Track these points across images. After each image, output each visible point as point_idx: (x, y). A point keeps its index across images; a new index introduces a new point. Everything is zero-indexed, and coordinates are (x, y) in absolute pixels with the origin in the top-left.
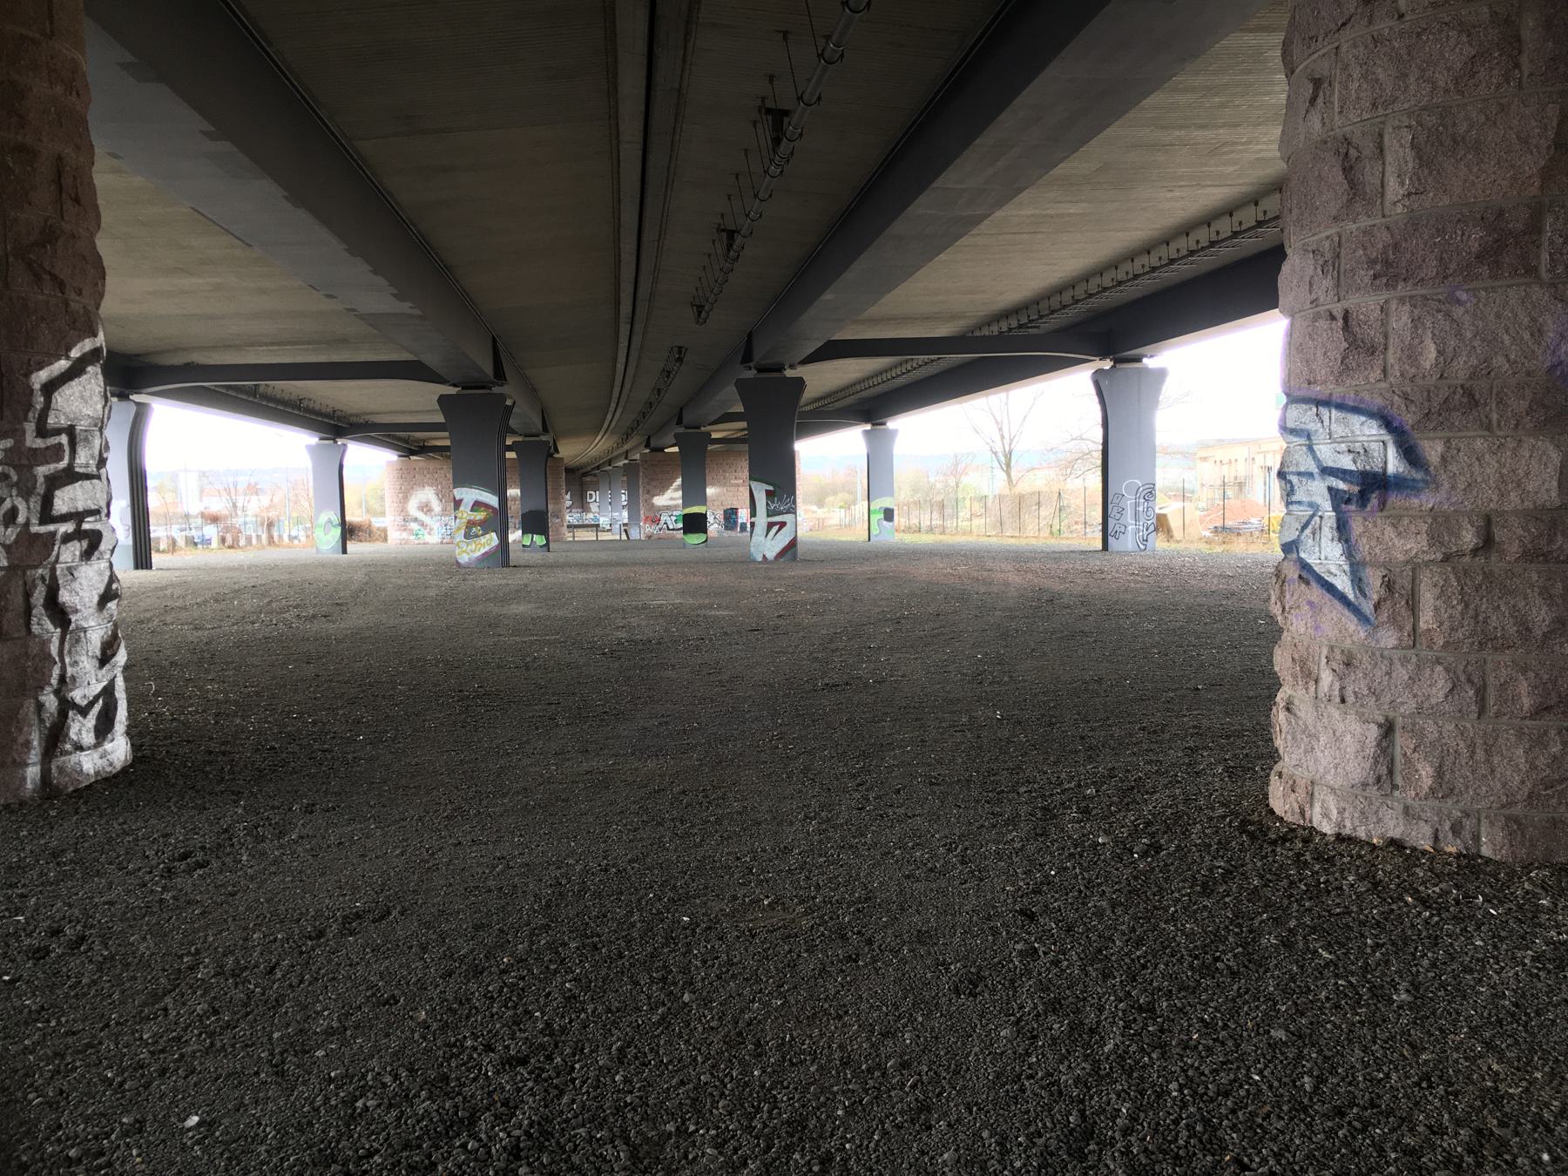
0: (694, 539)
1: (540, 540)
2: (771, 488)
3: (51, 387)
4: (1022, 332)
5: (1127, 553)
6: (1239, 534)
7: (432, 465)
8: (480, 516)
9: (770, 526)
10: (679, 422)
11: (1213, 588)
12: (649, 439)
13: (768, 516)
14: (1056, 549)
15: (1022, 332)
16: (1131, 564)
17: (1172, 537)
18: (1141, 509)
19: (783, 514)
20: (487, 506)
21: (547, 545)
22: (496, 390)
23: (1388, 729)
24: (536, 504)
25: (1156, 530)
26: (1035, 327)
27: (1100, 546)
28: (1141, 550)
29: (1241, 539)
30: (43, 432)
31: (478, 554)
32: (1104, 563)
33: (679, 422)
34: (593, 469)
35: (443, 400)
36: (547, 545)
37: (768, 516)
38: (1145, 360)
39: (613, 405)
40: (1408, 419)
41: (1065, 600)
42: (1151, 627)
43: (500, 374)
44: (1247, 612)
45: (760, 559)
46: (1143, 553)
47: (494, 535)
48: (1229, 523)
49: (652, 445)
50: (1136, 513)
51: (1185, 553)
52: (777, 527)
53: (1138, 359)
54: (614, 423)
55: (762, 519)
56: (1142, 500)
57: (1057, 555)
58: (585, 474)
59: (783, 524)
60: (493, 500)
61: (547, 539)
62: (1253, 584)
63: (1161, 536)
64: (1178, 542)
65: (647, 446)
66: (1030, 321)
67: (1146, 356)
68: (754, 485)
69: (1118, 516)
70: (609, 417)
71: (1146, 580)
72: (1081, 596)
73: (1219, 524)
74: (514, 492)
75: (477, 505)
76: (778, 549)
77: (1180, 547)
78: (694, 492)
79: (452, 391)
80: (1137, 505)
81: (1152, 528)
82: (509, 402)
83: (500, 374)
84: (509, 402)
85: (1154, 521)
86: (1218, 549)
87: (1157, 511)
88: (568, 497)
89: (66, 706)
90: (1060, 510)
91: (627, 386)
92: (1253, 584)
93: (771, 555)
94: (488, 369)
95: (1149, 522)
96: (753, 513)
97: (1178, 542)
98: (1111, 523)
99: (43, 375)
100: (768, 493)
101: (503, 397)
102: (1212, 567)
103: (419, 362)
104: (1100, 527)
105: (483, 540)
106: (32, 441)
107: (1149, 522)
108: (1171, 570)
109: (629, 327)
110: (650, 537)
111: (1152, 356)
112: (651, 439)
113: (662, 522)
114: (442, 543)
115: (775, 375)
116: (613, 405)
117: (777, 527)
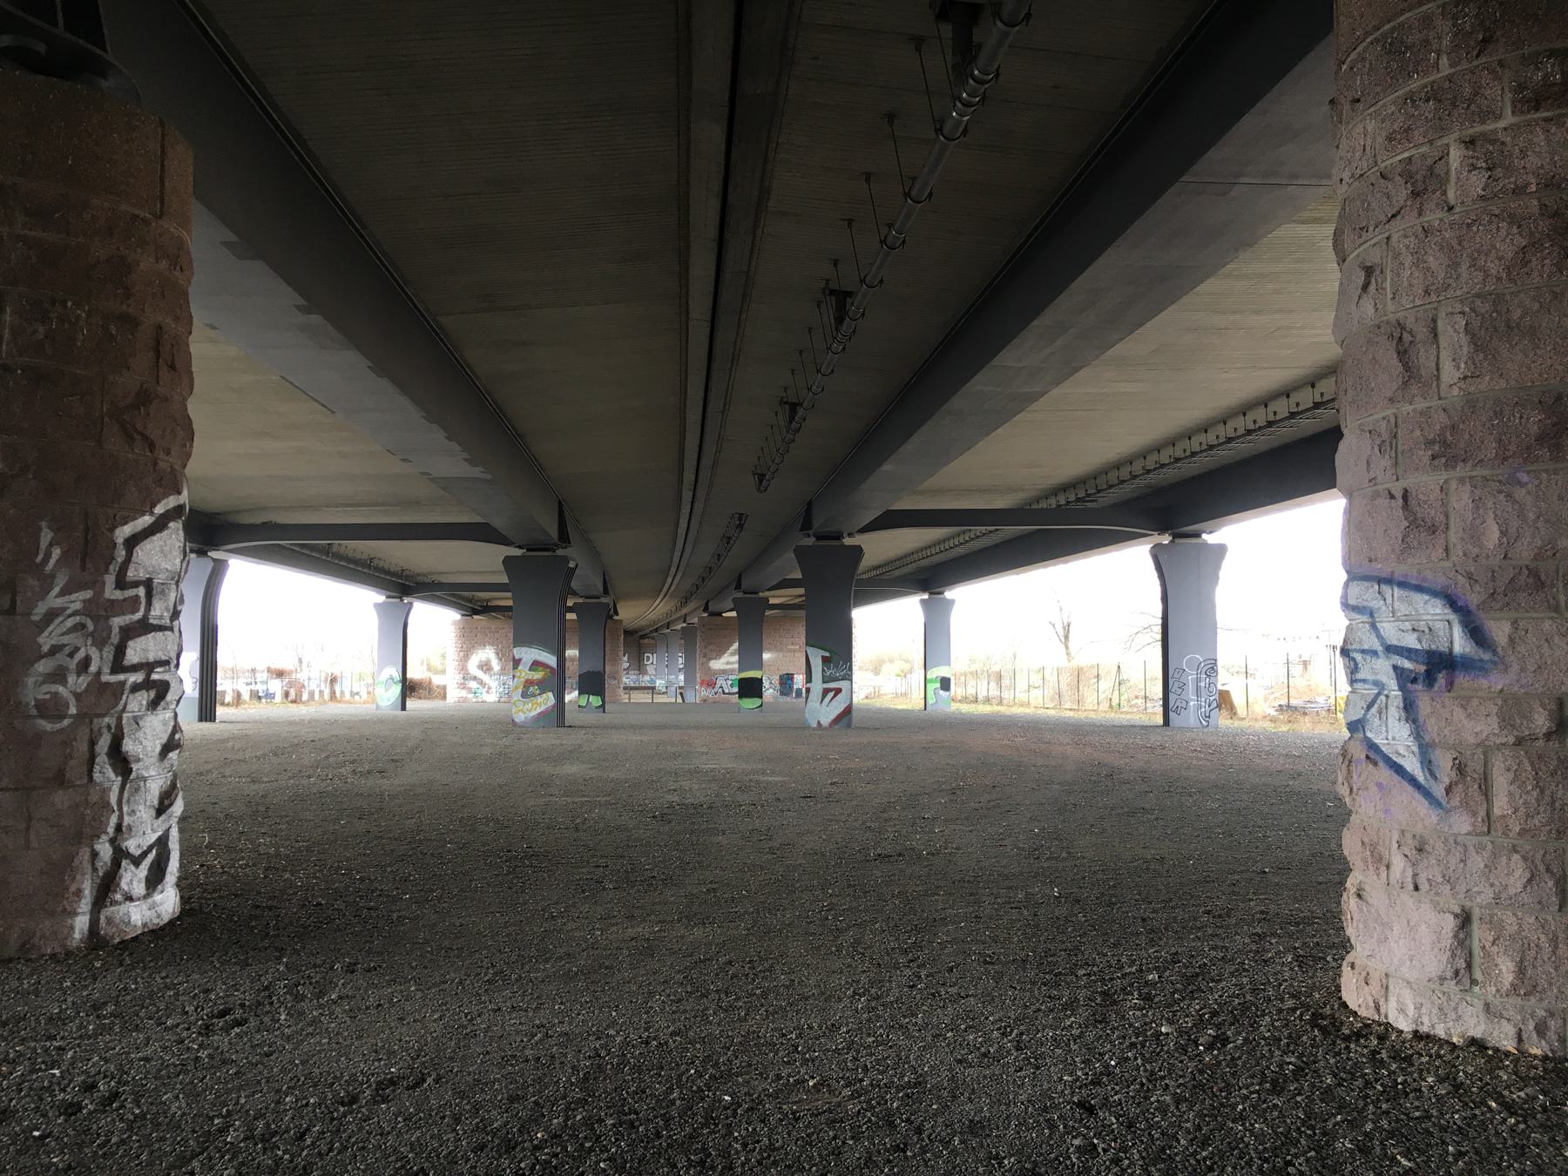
0: (750, 703)
1: (595, 701)
2: (827, 654)
3: (133, 542)
4: (1080, 506)
5: (1190, 729)
7: (494, 625)
8: (538, 675)
9: (826, 692)
10: (738, 587)
11: (1279, 768)
13: (824, 682)
14: (1115, 723)
15: (1080, 506)
16: (1193, 740)
17: (1235, 714)
18: (1203, 684)
19: (836, 680)
20: (545, 666)
21: (603, 706)
22: (560, 552)
24: (593, 666)
25: (1219, 706)
26: (1093, 501)
27: (1160, 720)
28: (1203, 727)
29: (1307, 719)
30: (121, 584)
31: (534, 713)
33: (738, 587)
35: (508, 561)
36: (603, 706)
37: (824, 682)
38: (1204, 536)
39: (673, 570)
40: (1473, 598)
43: (564, 538)
46: (1205, 730)
47: (550, 695)
48: (1294, 702)
50: (1198, 689)
52: (832, 694)
53: (1198, 535)
55: (817, 686)
57: (1116, 730)
58: (643, 637)
59: (838, 691)
60: (552, 660)
61: (603, 701)
62: (1320, 765)
63: (1224, 713)
64: (1243, 719)
65: (706, 610)
66: (1088, 495)
67: (1205, 532)
68: (811, 650)
69: (1179, 691)
70: (669, 580)
71: (1209, 757)
72: (1141, 772)
73: (1284, 702)
74: (572, 653)
75: (536, 665)
76: (833, 716)
77: (1244, 724)
78: (750, 656)
79: (518, 552)
80: (1198, 680)
81: (1214, 704)
82: (572, 565)
83: (564, 538)
84: (572, 565)
85: (1217, 697)
86: (1284, 728)
87: (1220, 687)
88: (626, 658)
89: (120, 854)
92: (1320, 765)
93: (826, 722)
94: (554, 533)
98: (1172, 697)
99: (126, 531)
100: (825, 659)
101: (566, 559)
102: (1278, 746)
105: (540, 699)
108: (1235, 747)
109: (691, 493)
110: (705, 701)
111: (1211, 532)
113: (718, 686)
114: (499, 701)
115: (836, 543)
116: (673, 570)
117: (832, 694)
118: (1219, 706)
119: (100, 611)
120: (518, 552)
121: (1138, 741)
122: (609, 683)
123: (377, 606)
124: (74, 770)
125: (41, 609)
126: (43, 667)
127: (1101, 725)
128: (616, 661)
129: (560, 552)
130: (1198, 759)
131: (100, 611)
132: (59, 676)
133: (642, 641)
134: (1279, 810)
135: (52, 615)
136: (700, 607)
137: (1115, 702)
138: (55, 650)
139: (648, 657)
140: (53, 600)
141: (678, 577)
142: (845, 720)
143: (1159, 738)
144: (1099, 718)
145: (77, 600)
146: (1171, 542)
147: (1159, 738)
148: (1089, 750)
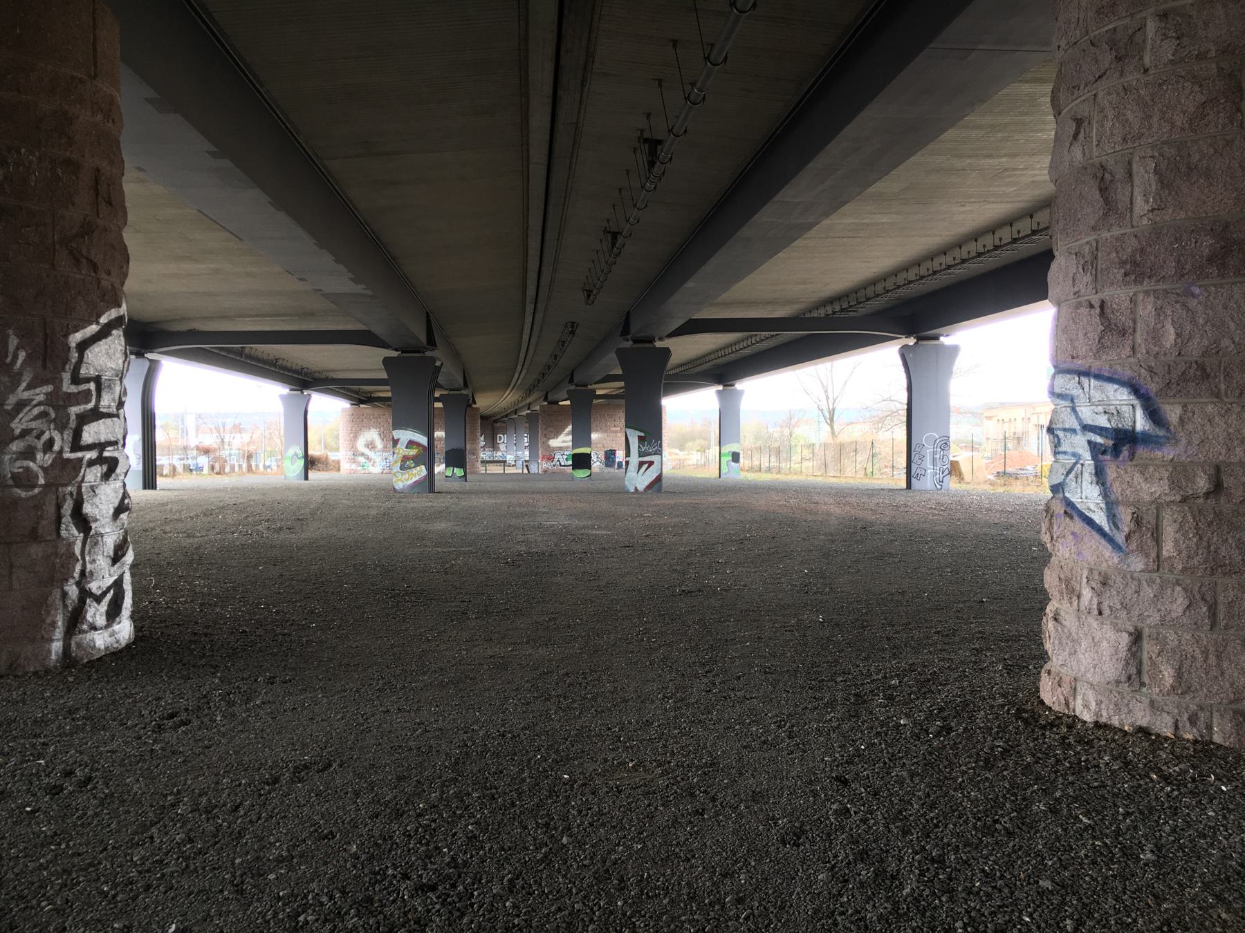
1: (459, 472)
2: (642, 434)
3: (84, 346)
5: (926, 491)
6: (1017, 478)
7: (377, 412)
8: (413, 452)
9: (641, 464)
10: (571, 381)
11: (996, 521)
12: (547, 393)
14: (870, 487)
16: (930, 500)
17: (963, 479)
18: (938, 456)
19: (650, 454)
20: (418, 445)
21: (465, 476)
22: (428, 354)
23: (1137, 637)
24: (456, 444)
25: (950, 473)
26: (854, 311)
27: (904, 486)
29: (1018, 482)
30: (76, 380)
31: (410, 482)
32: (908, 499)
33: (571, 381)
34: (503, 417)
35: (387, 361)
36: (465, 476)
37: (640, 456)
38: (942, 339)
39: (519, 367)
40: (1152, 387)
41: (876, 528)
42: (945, 551)
43: (431, 342)
44: (1023, 541)
45: (633, 491)
46: (939, 492)
47: (423, 467)
48: (1009, 470)
49: (549, 399)
50: (934, 460)
51: (973, 493)
52: (646, 465)
53: (936, 338)
54: (520, 381)
55: (635, 459)
56: (939, 450)
58: (496, 421)
59: (651, 463)
60: (423, 440)
61: (465, 472)
65: (546, 399)
66: (850, 306)
67: (942, 335)
68: (629, 431)
69: (919, 462)
73: (1001, 470)
74: (440, 434)
75: (411, 444)
76: (647, 483)
77: (970, 487)
78: (581, 436)
79: (395, 354)
80: (934, 453)
81: (947, 472)
82: (438, 364)
83: (431, 342)
84: (438, 364)
85: (949, 466)
86: (1001, 490)
87: (951, 459)
88: (482, 438)
89: (85, 594)
90: (873, 456)
91: (531, 352)
93: (641, 487)
95: (945, 467)
96: (628, 454)
97: (968, 483)
98: (914, 467)
101: (433, 359)
103: (369, 331)
104: (905, 471)
105: (414, 471)
106: (68, 387)
107: (945, 467)
109: (533, 306)
111: (947, 336)
112: (549, 395)
113: (556, 460)
114: (382, 473)
116: (519, 367)
117: (646, 465)
118: (950, 473)
119: (59, 402)
120: (395, 354)
121: (886, 501)
122: (469, 458)
123: (282, 397)
124: (46, 525)
125: (12, 400)
126: (15, 446)
127: (858, 489)
128: (475, 440)
129: (428, 354)
130: (933, 514)
131: (59, 402)
132: (29, 454)
133: (495, 425)
134: (995, 553)
135: (21, 405)
136: (540, 398)
137: (869, 471)
138: (25, 433)
139: (500, 438)
140: (22, 393)
141: (523, 373)
142: (656, 486)
143: (903, 499)
144: (857, 483)
145: (40, 393)
146: (915, 343)
147: (903, 499)
148: (848, 508)
